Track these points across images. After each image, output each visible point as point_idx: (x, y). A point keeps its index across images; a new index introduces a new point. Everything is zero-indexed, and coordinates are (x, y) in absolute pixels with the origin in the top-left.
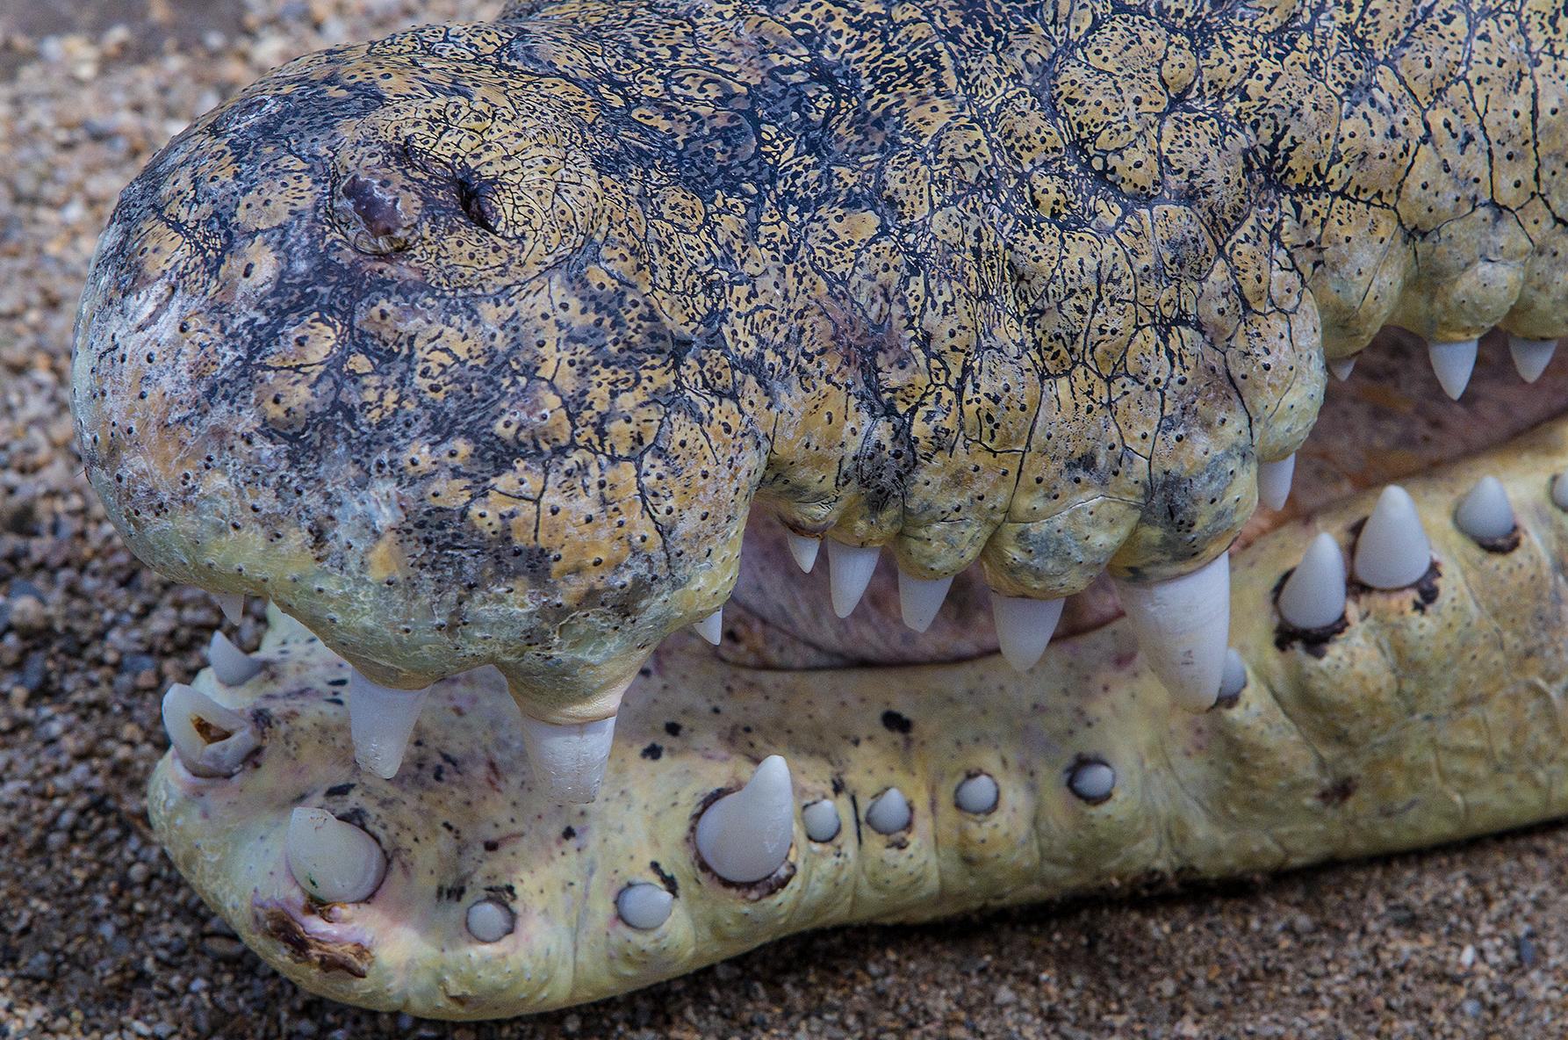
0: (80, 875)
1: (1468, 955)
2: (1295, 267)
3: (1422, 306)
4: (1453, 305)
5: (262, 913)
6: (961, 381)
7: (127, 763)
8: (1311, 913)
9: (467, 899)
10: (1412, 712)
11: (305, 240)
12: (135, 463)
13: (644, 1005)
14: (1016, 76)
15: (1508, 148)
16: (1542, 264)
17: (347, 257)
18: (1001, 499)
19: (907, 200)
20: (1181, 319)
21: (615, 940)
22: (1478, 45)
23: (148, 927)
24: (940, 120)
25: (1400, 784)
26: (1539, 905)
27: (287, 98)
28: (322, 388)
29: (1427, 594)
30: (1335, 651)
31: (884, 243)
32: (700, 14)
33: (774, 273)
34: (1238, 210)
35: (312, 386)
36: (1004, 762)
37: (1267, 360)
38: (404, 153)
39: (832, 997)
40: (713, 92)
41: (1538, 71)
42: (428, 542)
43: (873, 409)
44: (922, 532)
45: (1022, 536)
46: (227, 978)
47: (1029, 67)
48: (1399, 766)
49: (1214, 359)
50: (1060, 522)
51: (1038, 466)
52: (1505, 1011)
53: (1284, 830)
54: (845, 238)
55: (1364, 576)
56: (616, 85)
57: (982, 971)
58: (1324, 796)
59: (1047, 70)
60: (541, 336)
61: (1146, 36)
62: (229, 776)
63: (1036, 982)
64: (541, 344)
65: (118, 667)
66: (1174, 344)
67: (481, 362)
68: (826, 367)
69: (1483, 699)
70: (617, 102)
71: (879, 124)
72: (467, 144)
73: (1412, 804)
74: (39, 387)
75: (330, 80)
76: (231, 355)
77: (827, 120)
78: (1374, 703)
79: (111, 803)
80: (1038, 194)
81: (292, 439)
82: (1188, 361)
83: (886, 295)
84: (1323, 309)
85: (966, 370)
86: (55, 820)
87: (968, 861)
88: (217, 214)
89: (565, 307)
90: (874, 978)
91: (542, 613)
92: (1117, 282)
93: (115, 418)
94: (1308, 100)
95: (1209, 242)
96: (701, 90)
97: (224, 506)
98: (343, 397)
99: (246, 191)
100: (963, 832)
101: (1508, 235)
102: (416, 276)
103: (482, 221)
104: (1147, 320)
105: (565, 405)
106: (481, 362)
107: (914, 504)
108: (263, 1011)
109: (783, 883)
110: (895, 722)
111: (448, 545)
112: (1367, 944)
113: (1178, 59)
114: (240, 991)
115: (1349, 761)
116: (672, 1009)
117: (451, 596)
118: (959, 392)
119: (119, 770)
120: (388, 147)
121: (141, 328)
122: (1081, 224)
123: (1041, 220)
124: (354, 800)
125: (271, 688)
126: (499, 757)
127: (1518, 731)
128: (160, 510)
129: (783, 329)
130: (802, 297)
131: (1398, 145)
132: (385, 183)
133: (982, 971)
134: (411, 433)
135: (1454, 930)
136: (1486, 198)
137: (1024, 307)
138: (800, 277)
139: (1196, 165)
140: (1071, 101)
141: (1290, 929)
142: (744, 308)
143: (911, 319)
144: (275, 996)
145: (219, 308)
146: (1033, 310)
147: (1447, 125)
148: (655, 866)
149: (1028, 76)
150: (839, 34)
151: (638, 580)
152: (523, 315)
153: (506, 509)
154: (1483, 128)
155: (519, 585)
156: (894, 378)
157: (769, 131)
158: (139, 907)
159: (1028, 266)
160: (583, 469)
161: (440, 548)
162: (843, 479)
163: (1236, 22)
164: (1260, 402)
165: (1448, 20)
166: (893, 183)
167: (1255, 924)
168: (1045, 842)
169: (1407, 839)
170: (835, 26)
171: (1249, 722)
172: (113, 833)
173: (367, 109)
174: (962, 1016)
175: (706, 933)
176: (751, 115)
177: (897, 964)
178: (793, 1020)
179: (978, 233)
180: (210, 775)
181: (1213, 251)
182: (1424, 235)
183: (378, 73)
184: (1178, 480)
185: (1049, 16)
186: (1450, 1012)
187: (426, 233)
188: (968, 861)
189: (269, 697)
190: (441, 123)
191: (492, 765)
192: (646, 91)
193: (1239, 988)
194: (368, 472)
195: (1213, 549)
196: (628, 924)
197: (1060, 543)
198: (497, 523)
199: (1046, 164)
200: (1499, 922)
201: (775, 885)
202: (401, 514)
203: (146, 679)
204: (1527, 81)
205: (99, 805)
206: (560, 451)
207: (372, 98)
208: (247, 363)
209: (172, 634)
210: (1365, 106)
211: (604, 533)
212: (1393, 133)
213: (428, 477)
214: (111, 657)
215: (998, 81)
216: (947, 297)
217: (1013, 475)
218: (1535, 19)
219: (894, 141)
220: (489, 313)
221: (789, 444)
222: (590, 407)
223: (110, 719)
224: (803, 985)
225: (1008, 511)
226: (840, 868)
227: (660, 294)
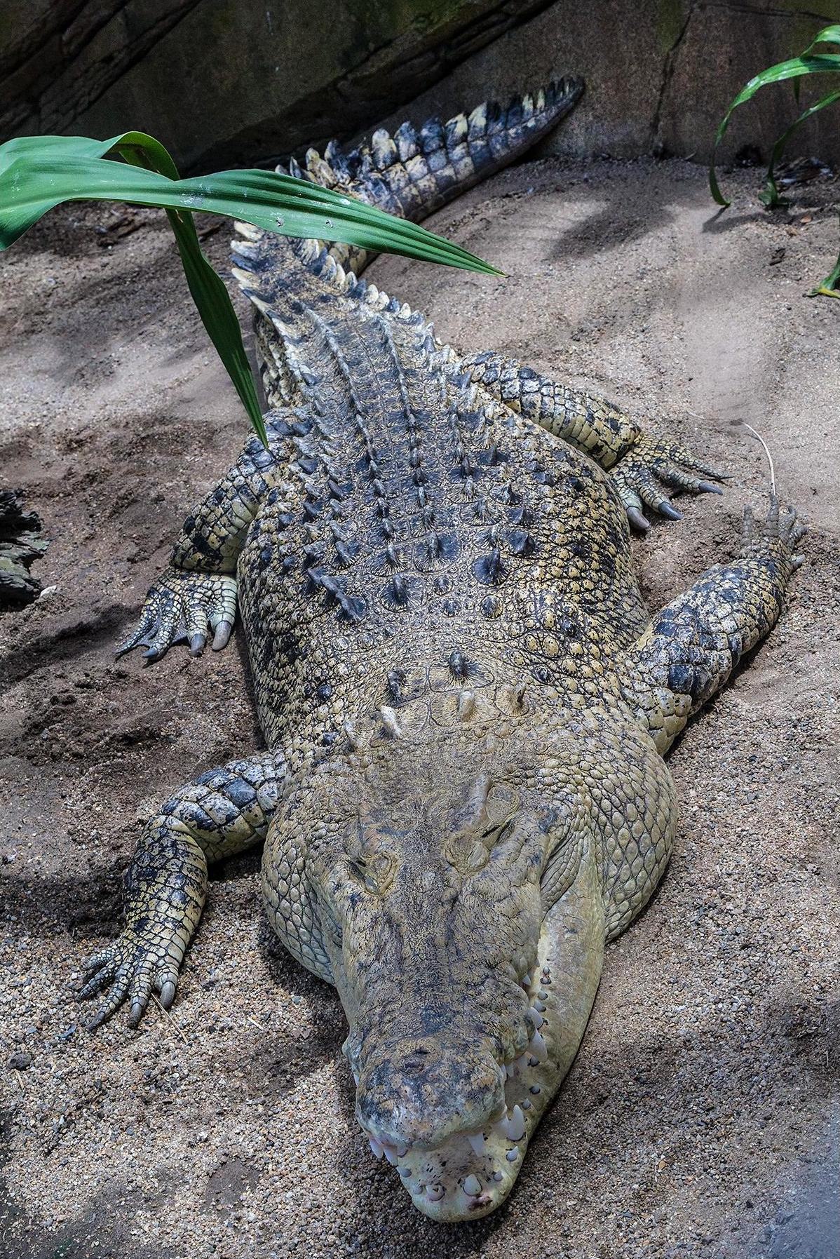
17: (417, 1075)
65: (382, 1232)
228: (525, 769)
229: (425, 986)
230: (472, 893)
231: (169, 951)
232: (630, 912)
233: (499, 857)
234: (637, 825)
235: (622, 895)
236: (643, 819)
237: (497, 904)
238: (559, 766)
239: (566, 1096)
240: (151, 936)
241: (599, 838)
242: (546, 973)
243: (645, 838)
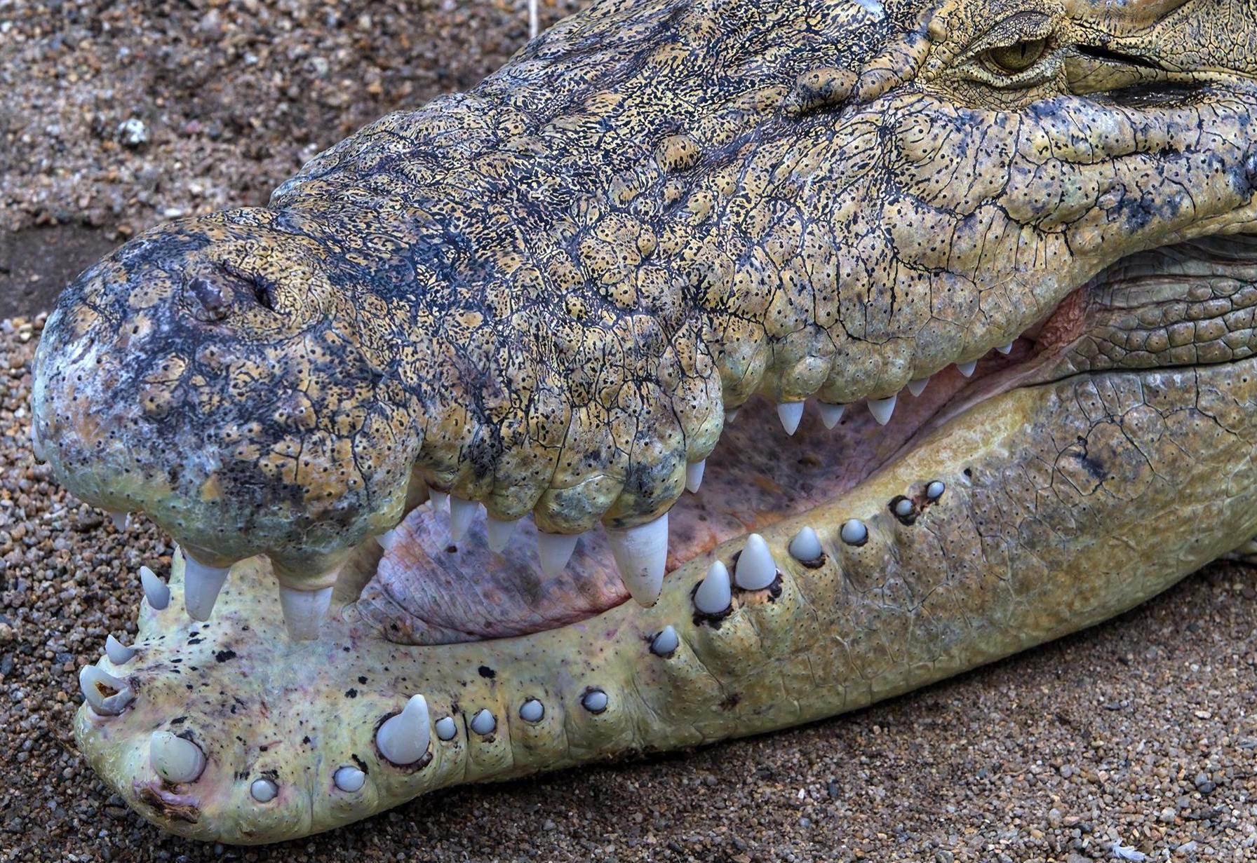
1: (802, 793)
2: (709, 353)
4: (792, 381)
5: (138, 789)
6: (528, 407)
8: (715, 774)
9: (251, 778)
10: (769, 657)
11: (168, 314)
12: (70, 436)
13: (350, 837)
14: (558, 243)
15: (824, 294)
16: (840, 360)
18: (548, 474)
19: (498, 307)
20: (648, 378)
21: (334, 797)
22: (807, 237)
23: (75, 803)
25: (764, 696)
26: (838, 765)
27: (155, 241)
28: (177, 393)
29: (775, 592)
30: (726, 625)
31: (486, 329)
32: (381, 207)
33: (426, 342)
34: (678, 320)
35: (172, 392)
36: (547, 692)
37: (694, 403)
38: (223, 268)
39: (454, 829)
40: (390, 246)
41: (840, 253)
42: (235, 480)
43: (480, 419)
44: (504, 492)
45: (558, 497)
46: (119, 829)
47: (565, 238)
48: (763, 687)
49: (665, 400)
50: (579, 488)
51: (570, 457)
52: (823, 823)
53: (702, 724)
54: (465, 325)
55: (740, 583)
56: (336, 242)
57: (536, 812)
58: (722, 704)
59: (574, 241)
60: (300, 367)
61: (629, 224)
62: (118, 714)
63: (566, 817)
64: (300, 372)
65: (53, 660)
66: (644, 392)
67: (266, 381)
68: (455, 394)
69: (807, 648)
70: (337, 250)
71: (482, 266)
72: (259, 263)
73: (771, 707)
75: (178, 233)
76: (125, 376)
77: (453, 264)
78: (748, 652)
79: (52, 735)
80: (570, 306)
81: (160, 421)
82: (651, 401)
83: (487, 357)
85: (531, 400)
86: (21, 745)
87: (528, 747)
88: (117, 301)
89: (313, 352)
90: (477, 818)
91: (297, 523)
92: (614, 355)
93: (59, 412)
94: (717, 262)
95: (663, 336)
96: (384, 245)
97: (121, 459)
98: (189, 399)
99: (133, 288)
100: (525, 732)
101: (822, 343)
102: (230, 333)
104: (630, 378)
105: (313, 405)
106: (266, 381)
107: (500, 475)
108: (139, 847)
109: (426, 764)
110: (486, 672)
111: (247, 482)
112: (746, 790)
113: (647, 237)
114: (127, 836)
115: (735, 685)
116: (366, 838)
117: (247, 511)
118: (527, 413)
119: (55, 717)
120: (214, 264)
121: (74, 362)
122: (594, 324)
123: (571, 320)
124: (187, 725)
125: (139, 665)
126: (266, 699)
128: (84, 461)
129: (432, 372)
130: (442, 356)
131: (766, 288)
132: (213, 282)
133: (536, 812)
134: (227, 419)
135: (794, 780)
136: (811, 321)
137: (562, 367)
138: (440, 345)
139: (657, 294)
140: (588, 257)
141: (704, 783)
142: (410, 359)
143: (501, 371)
144: (146, 838)
146: (567, 369)
147: (792, 279)
148: (355, 757)
149: (564, 243)
150: (459, 219)
151: (351, 507)
152: (290, 356)
153: (280, 462)
154: (811, 282)
156: (492, 403)
157: (422, 268)
158: (69, 791)
159: (564, 344)
160: (323, 441)
161: (242, 484)
162: (462, 458)
163: (677, 219)
164: (690, 427)
165: (791, 224)
166: (491, 297)
167: (685, 781)
168: (571, 736)
169: (769, 726)
170: (457, 215)
171: (680, 666)
172: (53, 751)
173: (200, 247)
174: (527, 837)
175: (384, 792)
177: (489, 809)
178: (433, 842)
179: (537, 326)
181: (665, 341)
182: (778, 340)
183: (206, 228)
184: (645, 468)
185: (575, 212)
186: (793, 825)
187: (236, 310)
188: (528, 747)
189: (139, 670)
190: (242, 252)
191: (263, 704)
192: (353, 245)
193: (677, 816)
194: (202, 440)
195: (662, 509)
196: (340, 789)
197: (579, 500)
198: (274, 469)
199: (574, 291)
200: (817, 776)
202: (221, 464)
203: (69, 666)
204: (834, 258)
205: (45, 736)
206: (310, 431)
207: (202, 241)
208: (134, 380)
209: (82, 641)
210: (748, 267)
211: (333, 478)
212: (762, 282)
213: (236, 443)
214: (49, 655)
215: (548, 246)
216: (521, 359)
217: (555, 460)
218: (838, 225)
219: (491, 276)
220: (271, 354)
221: (435, 434)
222: (327, 407)
223: (49, 688)
224: (437, 823)
226: (457, 754)
227: (365, 348)
230: (884, 131)
233: (1047, 122)
237: (906, 205)
239: (699, 777)
242: (927, 497)
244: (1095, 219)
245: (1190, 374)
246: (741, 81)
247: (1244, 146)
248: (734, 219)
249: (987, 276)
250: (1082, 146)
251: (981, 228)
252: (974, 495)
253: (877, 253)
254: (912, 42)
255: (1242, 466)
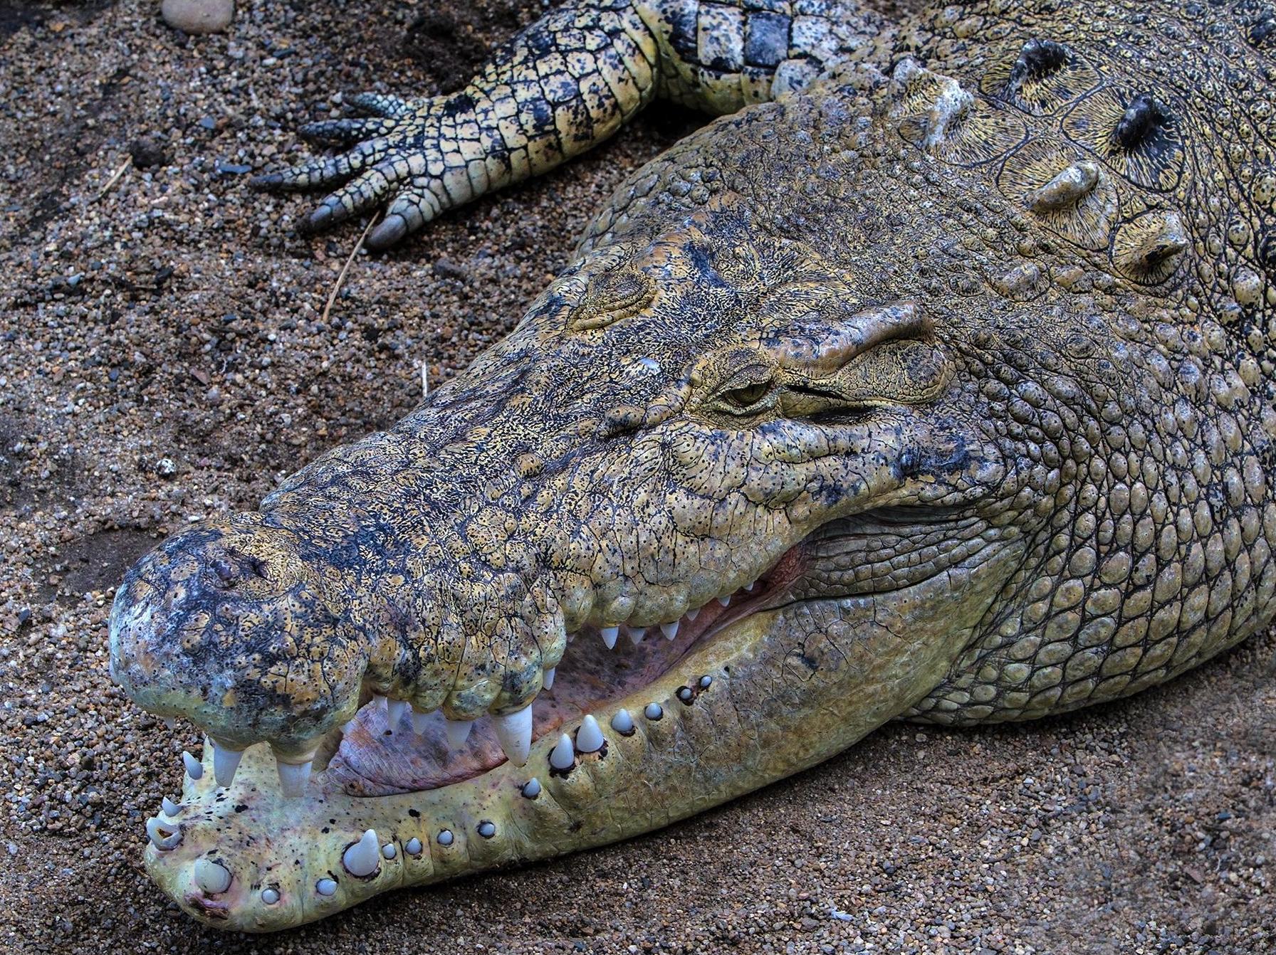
0: (120, 891)
1: (625, 885)
3: (599, 614)
7: (134, 849)
9: (262, 888)
12: (135, 667)
14: (452, 528)
18: (451, 681)
20: (515, 615)
24: (425, 543)
29: (603, 752)
30: (572, 776)
38: (232, 552)
45: (459, 696)
49: (528, 629)
50: (473, 690)
55: (580, 748)
56: (305, 532)
58: (571, 829)
65: (128, 815)
71: (403, 544)
72: (254, 550)
74: (92, 716)
78: (587, 794)
84: (565, 613)
85: (439, 632)
87: (443, 862)
101: (629, 587)
103: (260, 575)
107: (420, 683)
109: (377, 875)
110: (414, 813)
117: (254, 713)
118: (436, 641)
119: (131, 852)
122: (478, 580)
124: (218, 855)
127: (639, 800)
128: (145, 684)
135: (620, 877)
141: (561, 881)
145: (165, 610)
148: (329, 872)
155: (279, 708)
156: (412, 635)
160: (302, 665)
164: (544, 646)
166: (409, 565)
176: (355, 542)
180: (165, 849)
188: (443, 862)
201: (373, 876)
203: (138, 819)
205: (125, 865)
206: (294, 658)
212: (588, 548)
213: (245, 668)
214: (125, 811)
224: (385, 914)
225: (454, 686)
228: (1008, 360)
229: (427, 498)
230: (664, 446)
231: (447, 177)
232: (989, 709)
233: (770, 437)
234: (1109, 596)
235: (993, 673)
236: (1127, 595)
237: (681, 494)
238: (1068, 401)
240: (449, 133)
241: (1033, 562)
243: (1104, 625)
244: (805, 499)
245: (870, 599)
246: (568, 416)
247: (899, 448)
248: (568, 507)
249: (736, 539)
250: (794, 451)
251: (730, 508)
252: (731, 684)
253: (663, 526)
254: (679, 387)
255: (905, 659)
